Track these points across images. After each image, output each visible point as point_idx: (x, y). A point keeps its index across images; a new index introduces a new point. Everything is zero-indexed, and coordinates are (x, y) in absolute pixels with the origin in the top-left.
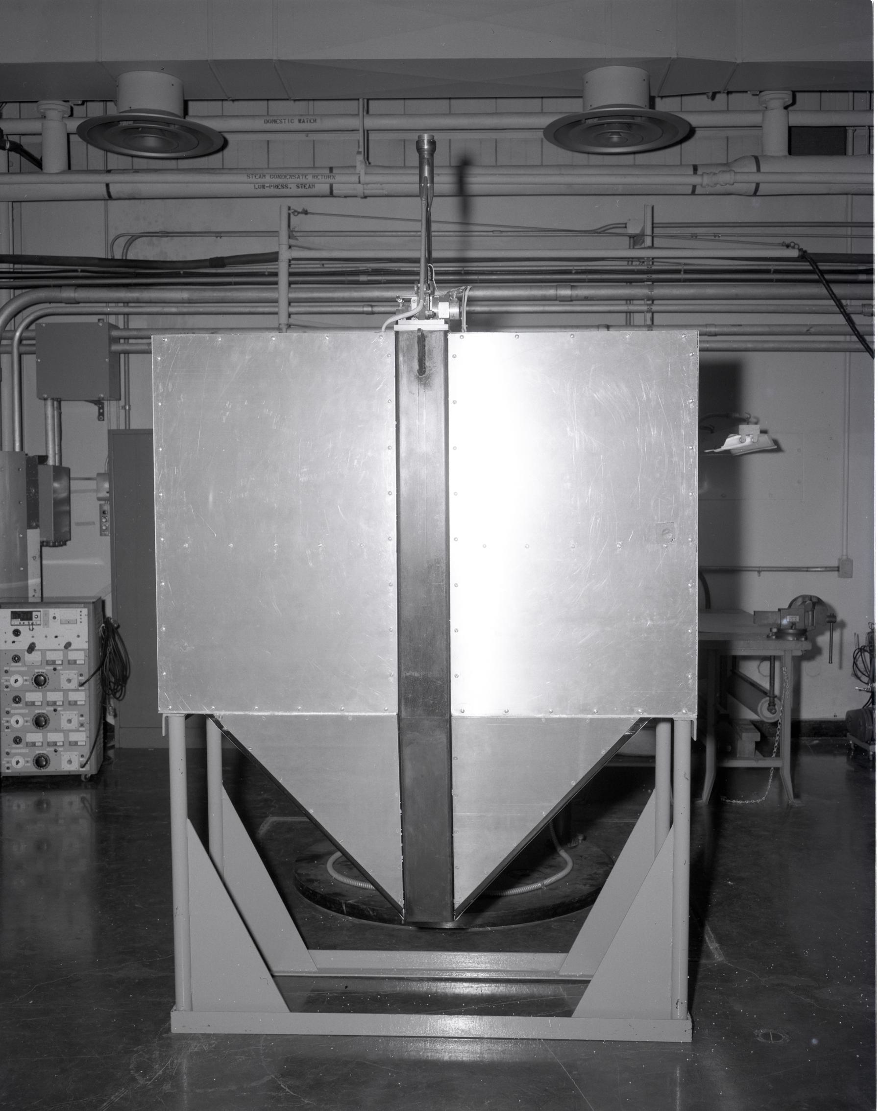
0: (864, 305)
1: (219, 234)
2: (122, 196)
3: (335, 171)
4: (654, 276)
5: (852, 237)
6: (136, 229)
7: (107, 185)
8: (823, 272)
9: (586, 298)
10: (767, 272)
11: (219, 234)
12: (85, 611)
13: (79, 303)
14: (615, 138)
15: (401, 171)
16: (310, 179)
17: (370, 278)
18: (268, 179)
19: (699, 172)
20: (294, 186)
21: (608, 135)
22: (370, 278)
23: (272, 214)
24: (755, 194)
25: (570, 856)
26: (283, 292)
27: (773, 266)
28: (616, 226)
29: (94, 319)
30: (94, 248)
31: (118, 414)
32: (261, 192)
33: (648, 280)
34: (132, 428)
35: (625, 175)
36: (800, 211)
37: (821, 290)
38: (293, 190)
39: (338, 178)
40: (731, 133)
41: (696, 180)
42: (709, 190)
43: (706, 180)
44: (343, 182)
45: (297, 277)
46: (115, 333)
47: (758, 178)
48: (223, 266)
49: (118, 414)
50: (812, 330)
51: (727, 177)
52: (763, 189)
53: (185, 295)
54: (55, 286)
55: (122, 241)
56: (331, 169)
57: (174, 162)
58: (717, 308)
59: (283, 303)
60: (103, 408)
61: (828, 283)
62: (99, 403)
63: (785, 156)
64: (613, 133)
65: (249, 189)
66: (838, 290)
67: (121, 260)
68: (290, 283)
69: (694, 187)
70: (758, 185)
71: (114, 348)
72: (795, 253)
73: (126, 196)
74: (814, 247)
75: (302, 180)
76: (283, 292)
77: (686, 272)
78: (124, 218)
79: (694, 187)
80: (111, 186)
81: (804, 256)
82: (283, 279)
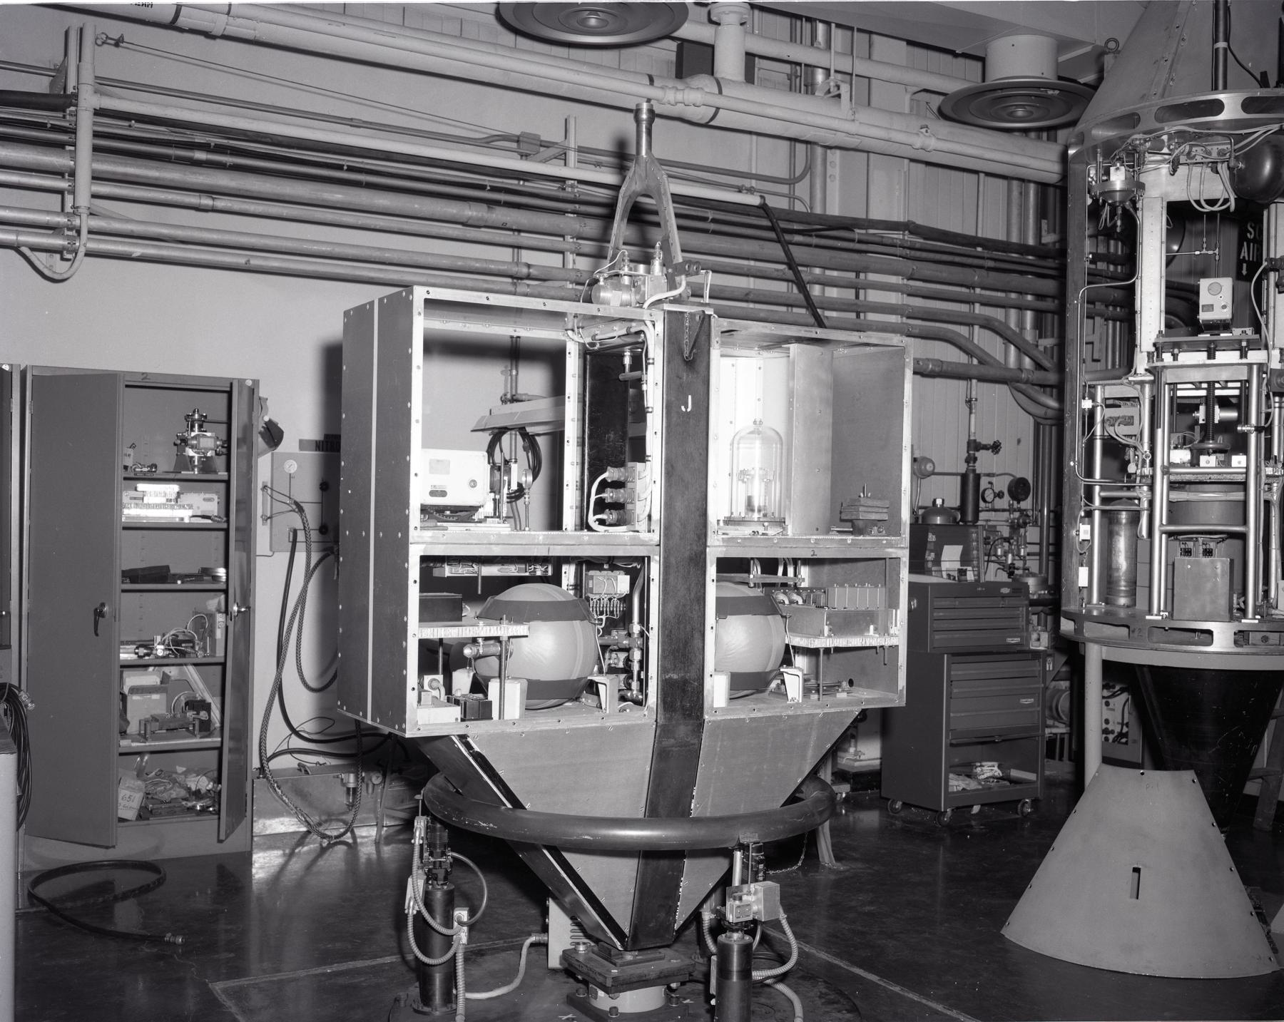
8: (772, 229)
12: (518, 686)
14: (1020, 112)
21: (1012, 109)
24: (706, 126)
25: (788, 986)
35: (578, 72)
37: (776, 250)
47: (719, 101)
50: (751, 297)
61: (785, 245)
63: (740, 83)
72: (754, 200)
76: (85, 162)
81: (763, 207)
82: (85, 140)
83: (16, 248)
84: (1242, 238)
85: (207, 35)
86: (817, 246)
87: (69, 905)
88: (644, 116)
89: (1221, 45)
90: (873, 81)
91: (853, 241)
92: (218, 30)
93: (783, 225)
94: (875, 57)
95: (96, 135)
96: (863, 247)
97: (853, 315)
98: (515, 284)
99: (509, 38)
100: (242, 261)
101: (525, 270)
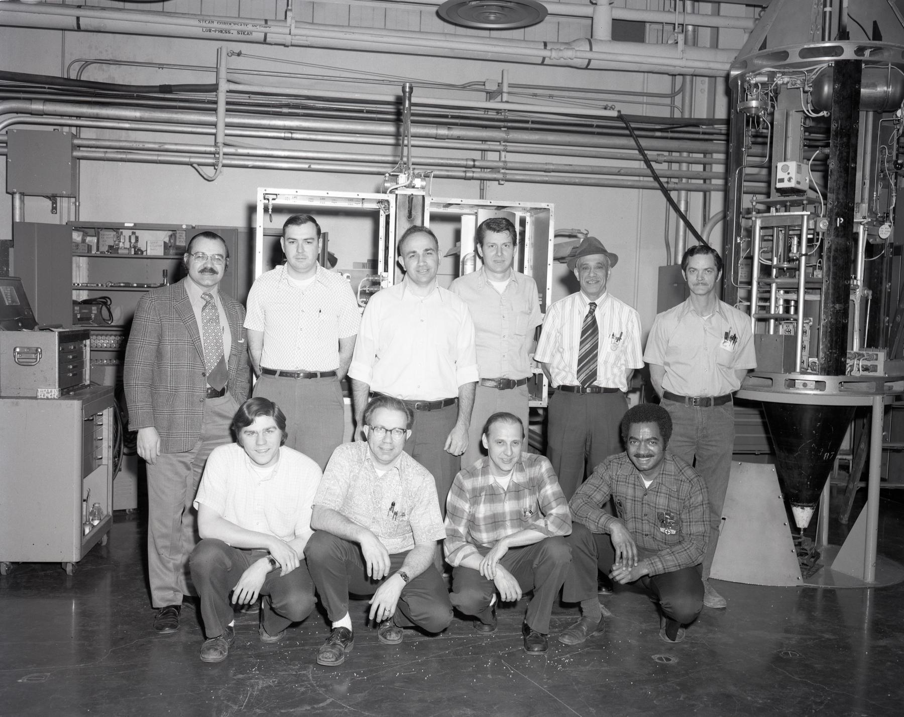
0: (658, 155)
1: (161, 66)
2: (90, 28)
3: (269, 23)
4: (509, 124)
5: (647, 104)
6: (92, 56)
7: (78, 18)
8: (627, 128)
9: (459, 138)
10: (446, 117)
11: (161, 66)
13: (80, 117)
14: (492, 17)
15: (308, 26)
16: (250, 28)
17: (290, 110)
18: (215, 25)
19: (549, 47)
20: (235, 32)
22: (290, 110)
23: (206, 53)
24: (586, 68)
26: (222, 118)
27: (595, 122)
28: (477, 83)
29: (51, 128)
30: (54, 70)
31: (69, 208)
32: (208, 35)
33: (504, 127)
34: (81, 220)
36: (611, 82)
37: (631, 142)
38: (234, 35)
39: (273, 29)
40: (423, 8)
41: (546, 53)
42: (555, 62)
43: (554, 54)
44: (276, 33)
45: (233, 108)
46: (76, 142)
47: (589, 55)
48: (170, 92)
49: (69, 208)
50: (622, 171)
51: (569, 53)
52: (547, 61)
53: (137, 114)
54: (25, 99)
55: (77, 66)
56: (266, 21)
57: (488, 32)
58: (535, 150)
59: (221, 125)
60: (56, 203)
61: (636, 138)
62: (53, 198)
64: (491, 13)
65: (198, 32)
66: (644, 143)
67: (76, 80)
68: (227, 110)
69: (544, 58)
70: (590, 61)
71: (76, 154)
72: (614, 114)
73: (92, 29)
74: (627, 110)
75: (243, 28)
77: (533, 122)
78: (80, 46)
79: (544, 58)
80: (81, 19)
81: (621, 118)
82: (222, 107)
83: (191, 165)
84: (53, 203)
85: (285, 46)
86: (672, 138)
87: (796, 678)
88: (407, 90)
89: (828, 9)
90: (720, 30)
91: (698, 133)
92: (288, 43)
93: (633, 125)
94: (722, 13)
95: (228, 103)
96: (706, 137)
97: (702, 182)
98: (465, 172)
99: (450, 28)
100: (306, 166)
101: (471, 163)
